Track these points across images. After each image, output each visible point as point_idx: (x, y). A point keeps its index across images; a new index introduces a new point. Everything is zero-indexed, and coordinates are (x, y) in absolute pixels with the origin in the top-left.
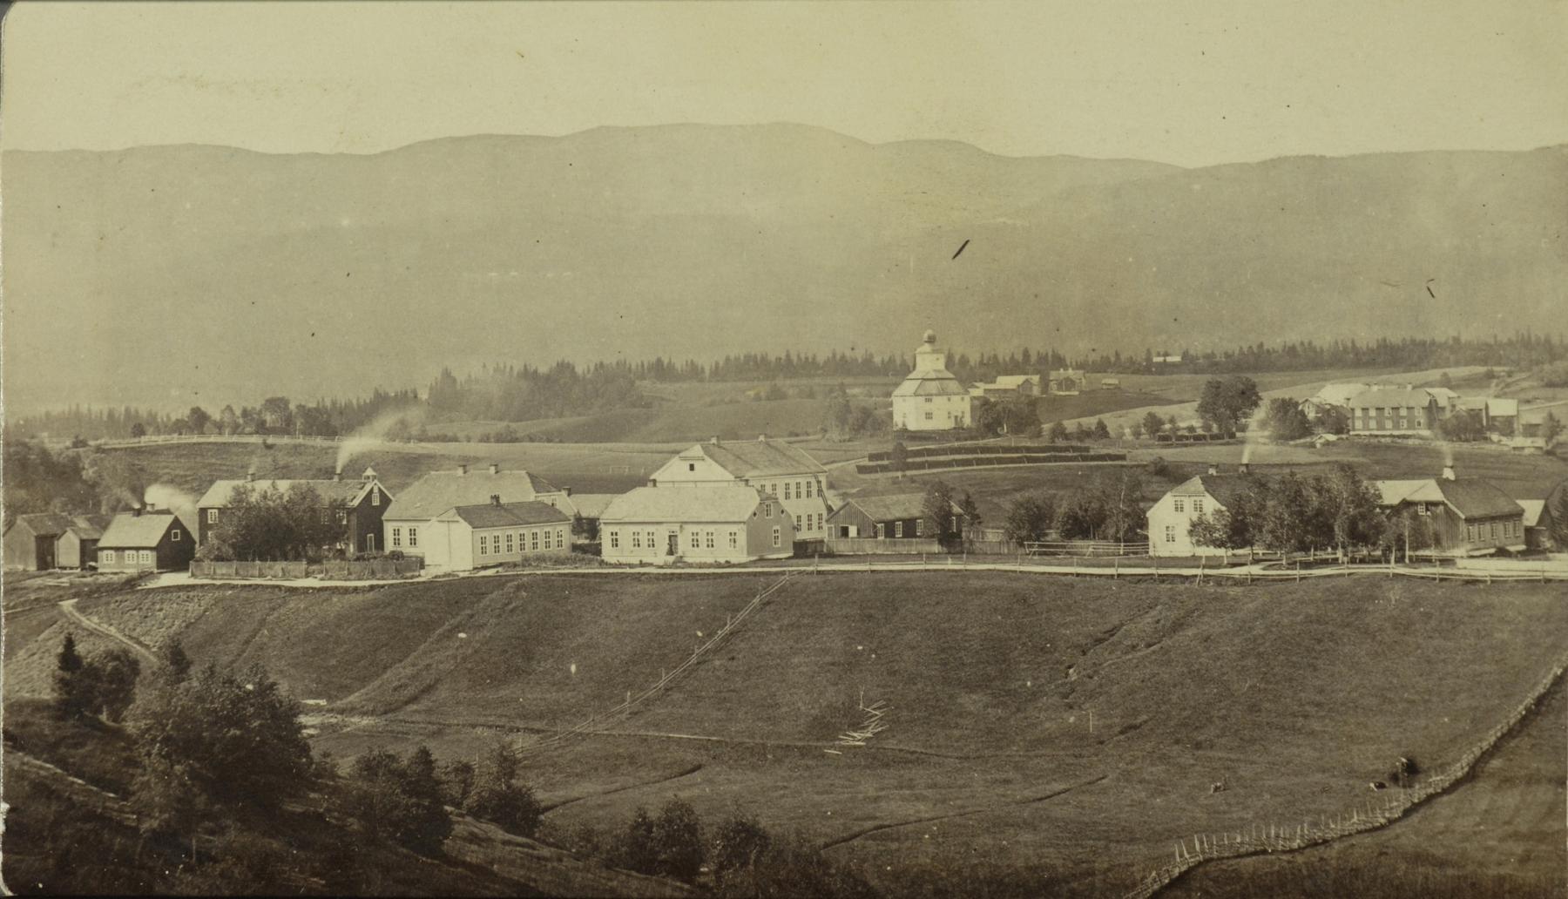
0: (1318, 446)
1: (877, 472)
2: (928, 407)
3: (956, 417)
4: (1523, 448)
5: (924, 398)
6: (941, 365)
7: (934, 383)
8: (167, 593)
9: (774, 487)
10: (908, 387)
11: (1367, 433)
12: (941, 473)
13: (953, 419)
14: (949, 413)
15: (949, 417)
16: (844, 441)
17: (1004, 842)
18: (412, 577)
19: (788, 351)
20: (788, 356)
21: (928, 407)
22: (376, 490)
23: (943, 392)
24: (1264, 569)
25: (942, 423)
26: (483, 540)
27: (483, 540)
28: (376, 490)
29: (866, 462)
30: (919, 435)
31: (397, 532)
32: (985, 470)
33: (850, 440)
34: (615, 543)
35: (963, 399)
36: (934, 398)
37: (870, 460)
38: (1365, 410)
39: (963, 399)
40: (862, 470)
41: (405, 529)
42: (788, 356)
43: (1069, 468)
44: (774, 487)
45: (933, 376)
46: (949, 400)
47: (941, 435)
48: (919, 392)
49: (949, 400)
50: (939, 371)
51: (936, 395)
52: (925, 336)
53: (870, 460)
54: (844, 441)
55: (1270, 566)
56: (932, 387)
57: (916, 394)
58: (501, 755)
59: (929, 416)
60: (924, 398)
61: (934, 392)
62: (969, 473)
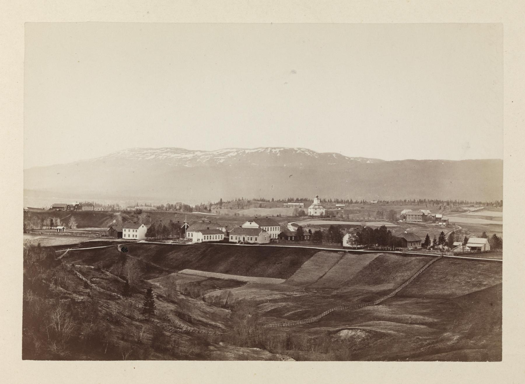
2: (316, 211)
6: (319, 202)
8: (441, 303)
9: (266, 228)
10: (312, 207)
11: (409, 220)
17: (216, 285)
18: (165, 242)
21: (316, 211)
22: (186, 225)
23: (319, 208)
24: (364, 250)
26: (205, 237)
27: (205, 237)
28: (186, 225)
31: (189, 234)
34: (232, 238)
41: (190, 233)
44: (266, 228)
45: (317, 204)
50: (319, 204)
52: (316, 196)
55: (371, 249)
56: (317, 207)
57: (313, 208)
59: (316, 213)
61: (317, 208)
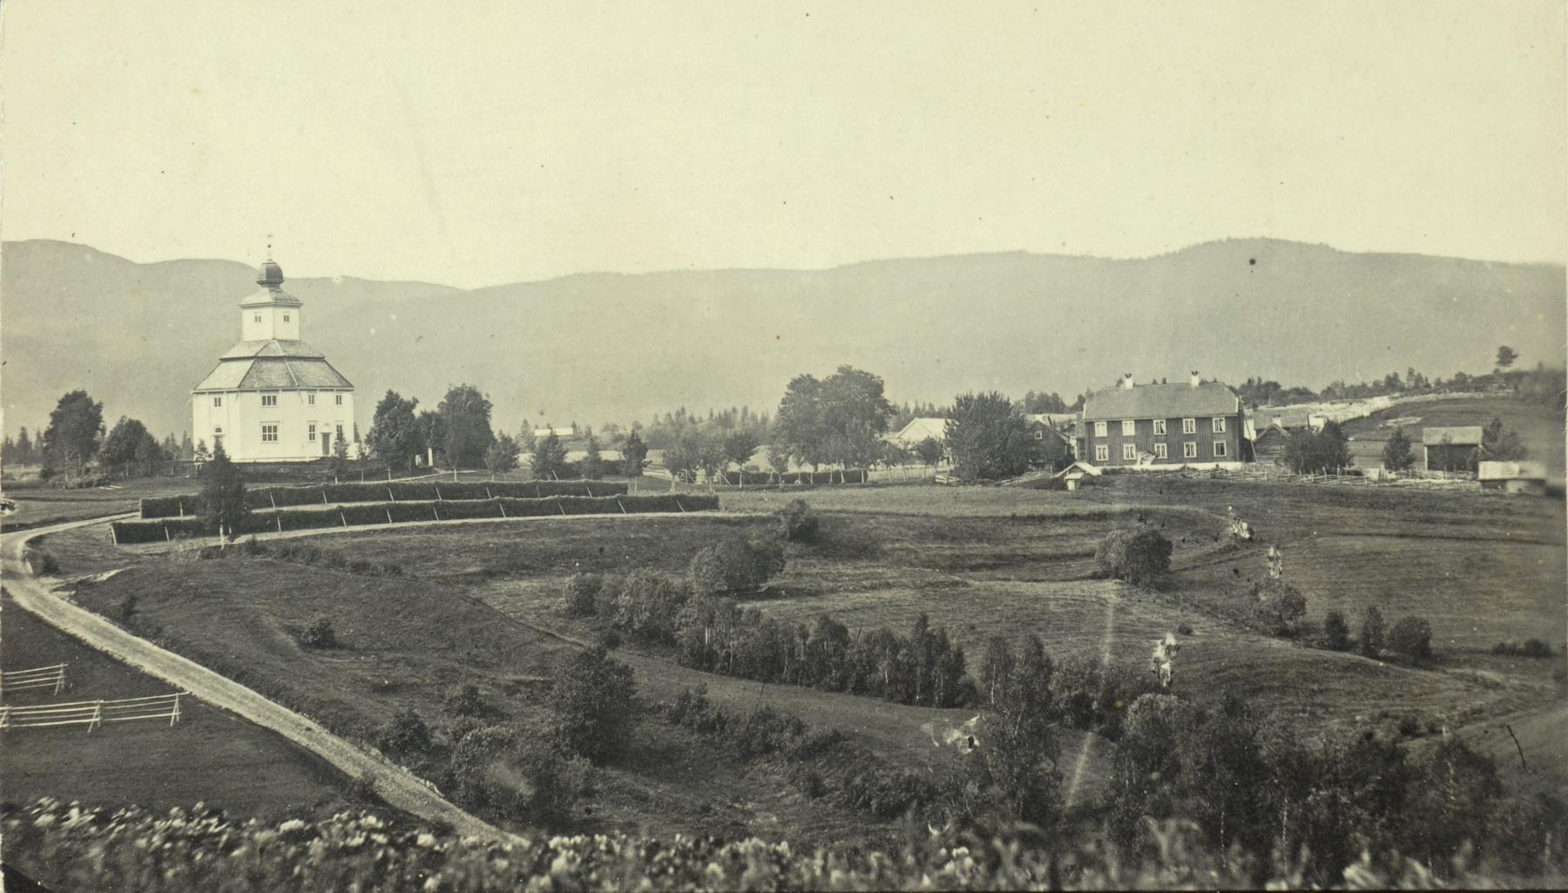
0: (1071, 485)
1: (163, 538)
2: (270, 415)
3: (326, 436)
4: (1503, 482)
5: (258, 397)
7: (279, 366)
12: (315, 537)
13: (319, 439)
14: (312, 428)
15: (312, 437)
16: (89, 485)
19: (23, 429)
20: (24, 435)
21: (270, 415)
25: (295, 447)
29: (137, 518)
30: (251, 470)
32: (419, 530)
33: (99, 483)
35: (339, 400)
36: (281, 396)
37: (146, 514)
38: (1115, 424)
39: (339, 400)
40: (126, 534)
42: (24, 435)
43: (609, 527)
46: (312, 401)
47: (297, 470)
48: (247, 385)
49: (312, 401)
51: (284, 390)
53: (146, 514)
54: (89, 485)
58: (197, 478)
60: (258, 397)
62: (379, 538)
